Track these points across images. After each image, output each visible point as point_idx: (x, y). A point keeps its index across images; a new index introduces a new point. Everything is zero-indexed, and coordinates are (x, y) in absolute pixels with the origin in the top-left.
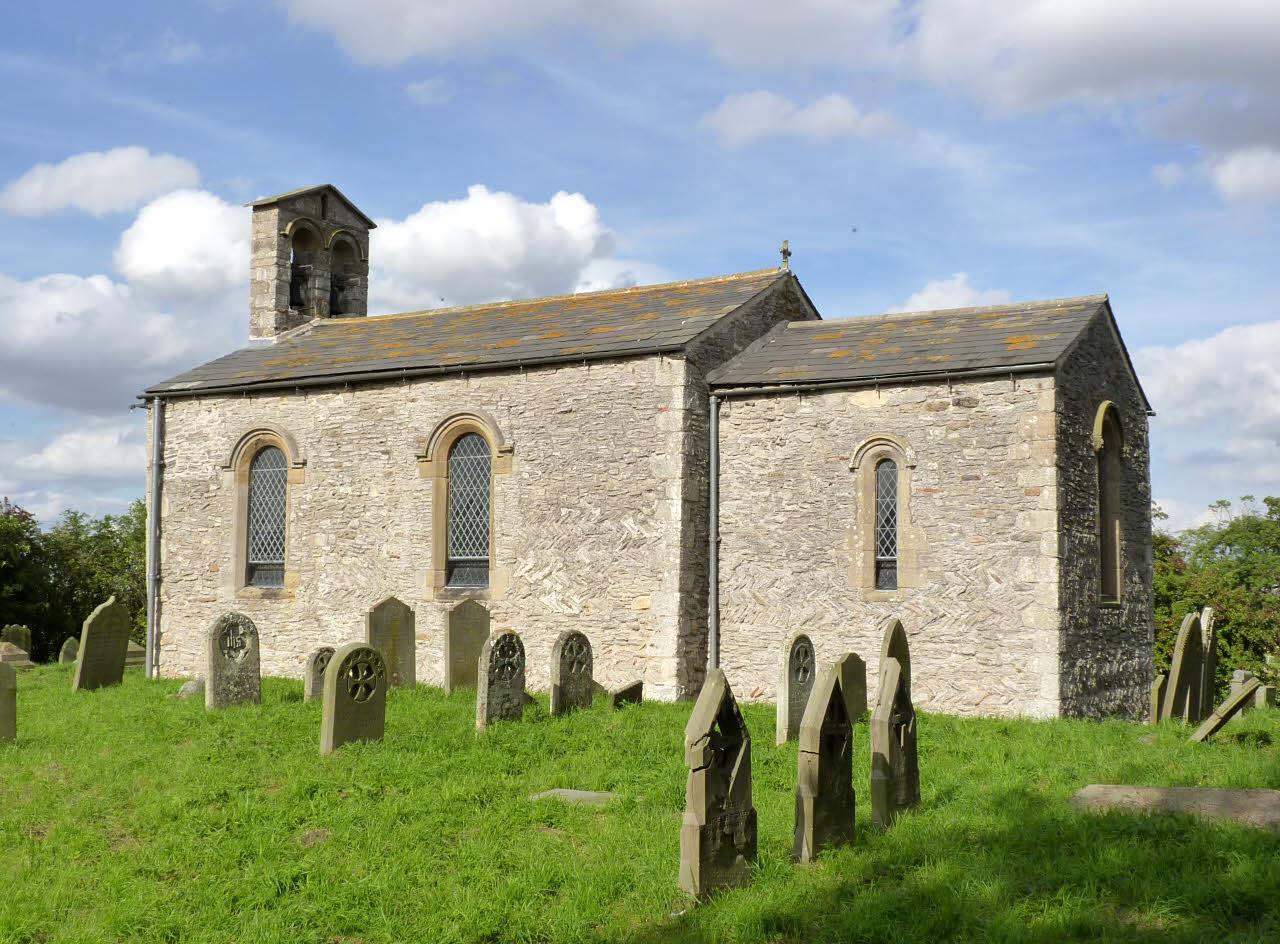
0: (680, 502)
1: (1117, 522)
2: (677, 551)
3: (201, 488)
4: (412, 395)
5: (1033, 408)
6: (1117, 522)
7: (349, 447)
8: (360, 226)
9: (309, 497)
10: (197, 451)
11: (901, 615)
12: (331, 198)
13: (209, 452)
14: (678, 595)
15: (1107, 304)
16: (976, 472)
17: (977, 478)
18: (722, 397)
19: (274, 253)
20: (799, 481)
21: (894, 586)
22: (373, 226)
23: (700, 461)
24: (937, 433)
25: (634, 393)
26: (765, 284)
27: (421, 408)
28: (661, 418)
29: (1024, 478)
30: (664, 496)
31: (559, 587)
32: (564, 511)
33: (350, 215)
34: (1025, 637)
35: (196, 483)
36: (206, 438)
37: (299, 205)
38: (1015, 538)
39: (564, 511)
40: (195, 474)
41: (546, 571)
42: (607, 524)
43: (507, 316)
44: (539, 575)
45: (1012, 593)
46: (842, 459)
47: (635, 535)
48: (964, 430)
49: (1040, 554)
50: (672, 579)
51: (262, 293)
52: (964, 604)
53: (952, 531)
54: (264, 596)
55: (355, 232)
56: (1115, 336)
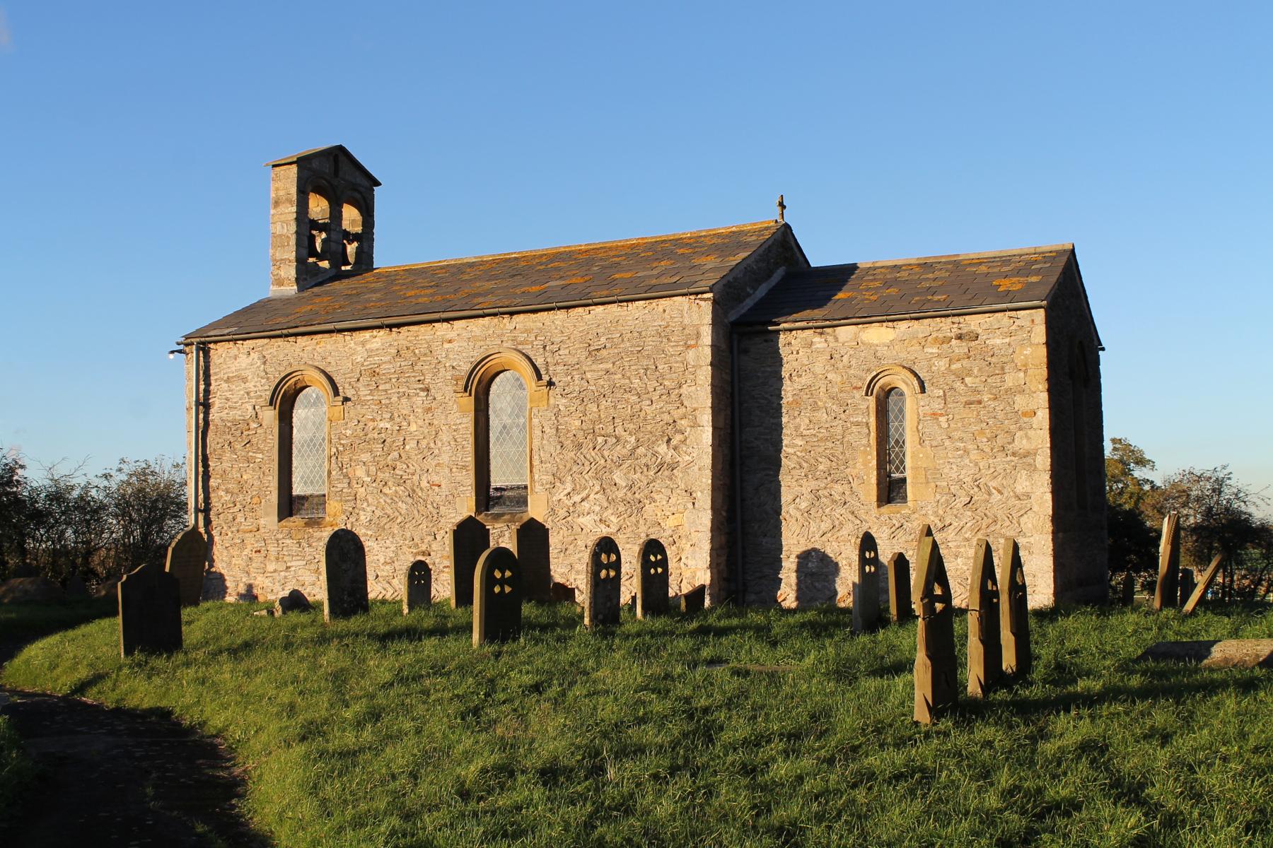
0: (710, 429)
1: (167, 570)
2: (708, 473)
3: (240, 428)
4: (452, 335)
5: (1024, 337)
6: (167, 570)
7: (388, 386)
8: (366, 183)
9: (349, 432)
10: (239, 389)
12: (342, 158)
13: (248, 393)
14: (710, 512)
15: (1073, 251)
17: (980, 402)
19: (294, 209)
20: (815, 408)
21: (904, 499)
22: (378, 184)
25: (664, 334)
26: (767, 235)
27: (459, 343)
28: (691, 354)
29: (1020, 402)
30: (695, 425)
31: (597, 508)
32: (600, 439)
33: (357, 173)
35: (236, 423)
36: (245, 380)
37: (315, 164)
38: (1014, 454)
39: (600, 439)
40: (236, 414)
41: (584, 494)
42: (641, 450)
43: (523, 264)
44: (577, 498)
45: (1013, 501)
46: (855, 388)
47: (668, 459)
48: (965, 362)
49: (1035, 469)
52: (969, 513)
53: (958, 449)
54: (307, 524)
55: (362, 189)
56: (798, 254)
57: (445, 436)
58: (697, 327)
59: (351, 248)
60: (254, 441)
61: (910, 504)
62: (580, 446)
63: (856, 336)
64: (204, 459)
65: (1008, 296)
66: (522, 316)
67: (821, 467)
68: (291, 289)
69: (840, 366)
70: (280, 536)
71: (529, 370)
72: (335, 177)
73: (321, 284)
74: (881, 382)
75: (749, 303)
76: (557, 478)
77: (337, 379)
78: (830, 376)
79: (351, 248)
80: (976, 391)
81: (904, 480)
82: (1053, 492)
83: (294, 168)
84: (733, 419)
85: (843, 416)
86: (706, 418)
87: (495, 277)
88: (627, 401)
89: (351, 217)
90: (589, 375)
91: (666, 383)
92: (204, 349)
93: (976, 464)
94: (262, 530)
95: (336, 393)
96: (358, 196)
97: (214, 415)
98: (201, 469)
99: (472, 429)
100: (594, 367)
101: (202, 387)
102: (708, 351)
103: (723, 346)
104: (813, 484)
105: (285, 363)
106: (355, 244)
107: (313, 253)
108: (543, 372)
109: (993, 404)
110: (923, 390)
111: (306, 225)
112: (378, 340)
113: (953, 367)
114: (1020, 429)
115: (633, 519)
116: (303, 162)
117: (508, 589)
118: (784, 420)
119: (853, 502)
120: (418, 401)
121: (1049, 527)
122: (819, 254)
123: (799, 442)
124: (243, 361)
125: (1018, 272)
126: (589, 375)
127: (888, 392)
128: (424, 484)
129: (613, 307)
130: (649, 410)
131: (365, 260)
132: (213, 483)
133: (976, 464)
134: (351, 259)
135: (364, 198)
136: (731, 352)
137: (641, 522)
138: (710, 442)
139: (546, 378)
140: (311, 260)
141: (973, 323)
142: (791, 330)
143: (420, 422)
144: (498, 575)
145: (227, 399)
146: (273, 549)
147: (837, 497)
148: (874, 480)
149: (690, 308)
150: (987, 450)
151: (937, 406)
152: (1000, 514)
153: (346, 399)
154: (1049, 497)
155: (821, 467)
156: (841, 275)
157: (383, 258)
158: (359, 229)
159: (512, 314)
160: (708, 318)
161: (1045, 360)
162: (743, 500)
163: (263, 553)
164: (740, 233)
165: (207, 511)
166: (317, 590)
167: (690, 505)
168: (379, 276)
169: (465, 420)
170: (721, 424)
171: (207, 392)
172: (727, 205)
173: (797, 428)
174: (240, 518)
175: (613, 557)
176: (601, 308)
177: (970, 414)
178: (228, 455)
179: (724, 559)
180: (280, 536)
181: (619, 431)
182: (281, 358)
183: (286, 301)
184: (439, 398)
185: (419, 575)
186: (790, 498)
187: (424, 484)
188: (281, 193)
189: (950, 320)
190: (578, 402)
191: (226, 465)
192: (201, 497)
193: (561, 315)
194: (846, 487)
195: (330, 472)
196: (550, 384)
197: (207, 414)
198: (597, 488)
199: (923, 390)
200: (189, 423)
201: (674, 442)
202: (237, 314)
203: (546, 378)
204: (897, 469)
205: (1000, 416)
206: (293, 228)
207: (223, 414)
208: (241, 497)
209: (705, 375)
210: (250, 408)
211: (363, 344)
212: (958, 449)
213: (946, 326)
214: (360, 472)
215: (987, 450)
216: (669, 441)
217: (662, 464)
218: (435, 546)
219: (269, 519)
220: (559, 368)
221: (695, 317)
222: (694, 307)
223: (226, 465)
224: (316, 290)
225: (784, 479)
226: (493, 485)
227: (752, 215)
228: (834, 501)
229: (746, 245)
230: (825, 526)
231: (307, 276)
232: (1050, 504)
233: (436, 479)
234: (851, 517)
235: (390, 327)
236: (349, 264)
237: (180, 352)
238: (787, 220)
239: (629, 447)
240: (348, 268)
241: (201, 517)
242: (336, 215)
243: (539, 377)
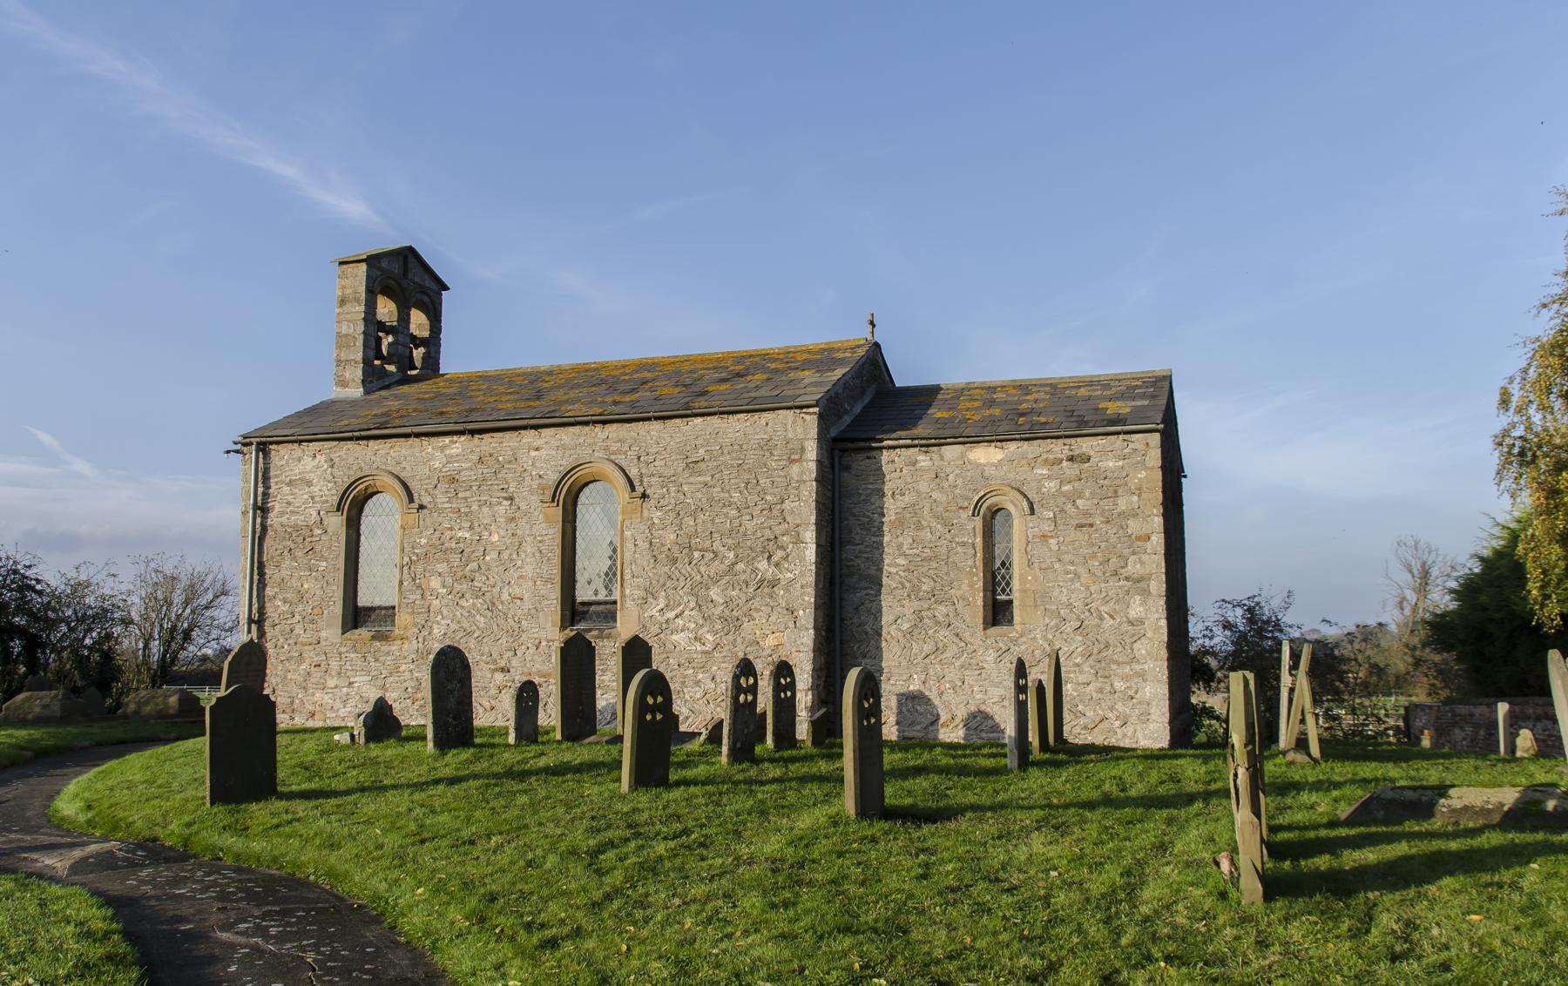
2: (811, 591)
3: (303, 535)
5: (1132, 461)
7: (468, 494)
8: (435, 287)
9: (423, 541)
10: (302, 494)
11: (1020, 650)
14: (812, 631)
16: (1090, 521)
17: (1091, 525)
18: (844, 451)
19: (363, 308)
20: (919, 528)
21: (1010, 622)
22: (446, 288)
23: (292, 796)
24: (1051, 485)
25: (767, 447)
27: (544, 454)
28: (795, 468)
29: (1134, 526)
30: (798, 540)
31: (692, 626)
32: (696, 554)
34: (1137, 667)
35: (297, 528)
36: (309, 483)
37: (384, 264)
38: (1127, 579)
40: (298, 519)
42: (741, 566)
44: (671, 615)
45: (1125, 627)
48: (1077, 484)
50: (806, 616)
51: (348, 347)
53: (1068, 573)
54: (373, 638)
57: (529, 548)
58: (801, 441)
59: (418, 353)
60: (318, 548)
61: (1018, 627)
62: (675, 561)
63: (963, 455)
64: (259, 568)
65: (1117, 420)
66: (615, 426)
67: (924, 588)
68: (357, 392)
69: (946, 485)
70: (343, 649)
71: (622, 481)
72: (403, 278)
73: (387, 387)
74: (988, 502)
75: (847, 419)
76: (650, 593)
77: (412, 485)
78: (935, 495)
79: (418, 353)
80: (1087, 514)
81: (1011, 602)
82: (1168, 618)
83: (364, 267)
84: (833, 537)
85: (948, 536)
86: (810, 535)
87: (578, 386)
88: (726, 515)
89: (418, 322)
90: (685, 488)
91: (768, 498)
92: (263, 448)
93: (1088, 588)
94: (323, 643)
95: (411, 500)
96: (426, 299)
97: (273, 519)
98: (256, 577)
99: (559, 541)
100: (692, 479)
101: (260, 490)
102: (813, 466)
103: (827, 463)
104: (916, 605)
105: (355, 467)
106: (422, 350)
107: (379, 356)
108: (636, 483)
109: (1105, 527)
110: (1032, 511)
111: (374, 326)
112: (457, 446)
113: (1065, 488)
114: (1134, 553)
115: (730, 637)
116: (372, 261)
117: (659, 717)
118: (886, 539)
119: (956, 623)
120: (501, 510)
121: (1164, 654)
122: (904, 376)
123: (901, 561)
124: (308, 463)
125: (1121, 397)
126: (685, 488)
127: (994, 512)
128: (505, 596)
129: (715, 420)
130: (749, 525)
131: (432, 365)
132: (269, 591)
133: (1088, 588)
134: (418, 363)
135: (433, 302)
136: (833, 467)
137: (739, 640)
138: (813, 559)
139: (639, 490)
140: (377, 362)
141: (1084, 445)
142: (894, 448)
143: (502, 532)
144: (650, 700)
145: (289, 503)
146: (334, 664)
147: (941, 619)
148: (980, 602)
149: (794, 422)
150: (1099, 574)
151: (1047, 527)
152: (1112, 640)
153: (422, 507)
154: (1163, 623)
155: (924, 588)
156: (927, 395)
157: (453, 362)
158: (426, 334)
159: (604, 422)
160: (814, 433)
161: (1160, 484)
162: (842, 620)
163: (323, 668)
164: (831, 350)
165: (260, 622)
166: (416, 713)
167: (791, 625)
168: (451, 381)
169: (551, 531)
170: (823, 542)
171: (266, 495)
172: (814, 319)
173: (900, 546)
174: (299, 630)
175: (751, 681)
176: (700, 420)
177: (1081, 536)
178: (287, 562)
179: (821, 682)
180: (343, 649)
181: (717, 545)
182: (351, 461)
183: (353, 403)
184: (523, 507)
185: (527, 695)
186: (891, 618)
187: (505, 596)
188: (348, 291)
189: (1061, 441)
190: (673, 515)
191: (285, 573)
192: (255, 606)
193: (656, 426)
194: (951, 609)
195: (401, 583)
196: (644, 496)
197: (264, 518)
198: (692, 604)
199: (1032, 511)
200: (244, 529)
201: (775, 559)
202: (298, 415)
203: (639, 490)
204: (1003, 591)
205: (1113, 539)
206: (361, 327)
207: (284, 519)
208: (300, 608)
209: (809, 491)
210: (314, 513)
211: (442, 449)
212: (1068, 573)
213: (1058, 448)
214: (435, 583)
215: (1099, 574)
216: (769, 557)
217: (762, 581)
218: (514, 663)
219: (331, 632)
220: (654, 479)
221: (801, 432)
222: (799, 421)
223: (285, 573)
224: (383, 393)
225: (886, 600)
226: (579, 599)
227: (848, 332)
228: (937, 623)
229: (842, 362)
230: (928, 648)
231: (374, 378)
232: (1165, 631)
233: (517, 591)
234: (956, 640)
235: (473, 432)
236: (415, 368)
237: (237, 452)
238: (878, 339)
239: (727, 562)
240: (414, 372)
241: (254, 627)
242: (404, 319)
243: (633, 488)
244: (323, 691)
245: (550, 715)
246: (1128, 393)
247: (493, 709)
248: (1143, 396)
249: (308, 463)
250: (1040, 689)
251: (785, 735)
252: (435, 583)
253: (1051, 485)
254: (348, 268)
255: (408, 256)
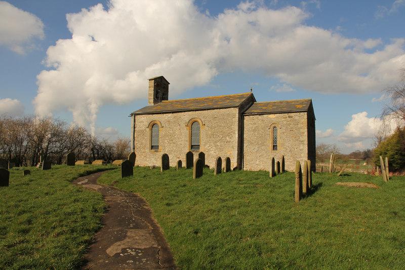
3: (142, 132)
21: (277, 150)
27: (186, 117)
28: (234, 119)
29: (301, 130)
86: (237, 132)
124: (143, 118)
125: (300, 104)
183: (151, 107)
185: (180, 163)
219: (148, 150)
229: (245, 98)
244: (146, 160)
245: (184, 164)
246: (302, 103)
247: (173, 163)
248: (305, 104)
249: (143, 118)
250: (278, 163)
251: (228, 168)
252: (166, 141)
253: (285, 122)
254: (151, 81)
255: (162, 78)
